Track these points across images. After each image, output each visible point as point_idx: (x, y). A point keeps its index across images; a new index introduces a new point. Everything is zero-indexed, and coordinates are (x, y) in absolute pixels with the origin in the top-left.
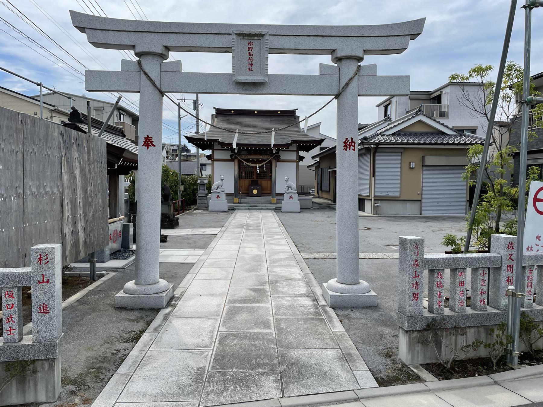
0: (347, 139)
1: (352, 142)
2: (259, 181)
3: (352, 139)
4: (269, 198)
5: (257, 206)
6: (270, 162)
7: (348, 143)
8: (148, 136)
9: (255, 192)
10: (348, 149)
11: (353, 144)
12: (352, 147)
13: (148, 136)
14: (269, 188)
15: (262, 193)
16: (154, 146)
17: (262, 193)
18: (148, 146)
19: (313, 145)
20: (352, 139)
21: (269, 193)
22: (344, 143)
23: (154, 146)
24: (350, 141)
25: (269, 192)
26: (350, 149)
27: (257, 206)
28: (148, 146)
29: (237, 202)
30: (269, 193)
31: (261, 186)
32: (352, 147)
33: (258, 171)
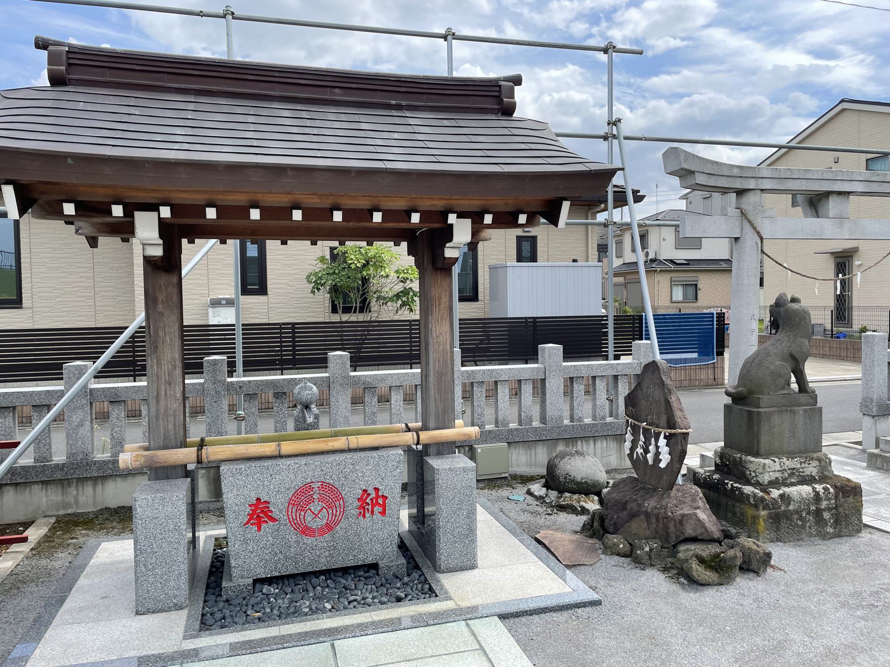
1: (377, 496)
7: (368, 501)
8: (258, 499)
11: (380, 501)
13: (258, 499)
16: (273, 519)
20: (377, 490)
26: (372, 513)
32: (377, 509)
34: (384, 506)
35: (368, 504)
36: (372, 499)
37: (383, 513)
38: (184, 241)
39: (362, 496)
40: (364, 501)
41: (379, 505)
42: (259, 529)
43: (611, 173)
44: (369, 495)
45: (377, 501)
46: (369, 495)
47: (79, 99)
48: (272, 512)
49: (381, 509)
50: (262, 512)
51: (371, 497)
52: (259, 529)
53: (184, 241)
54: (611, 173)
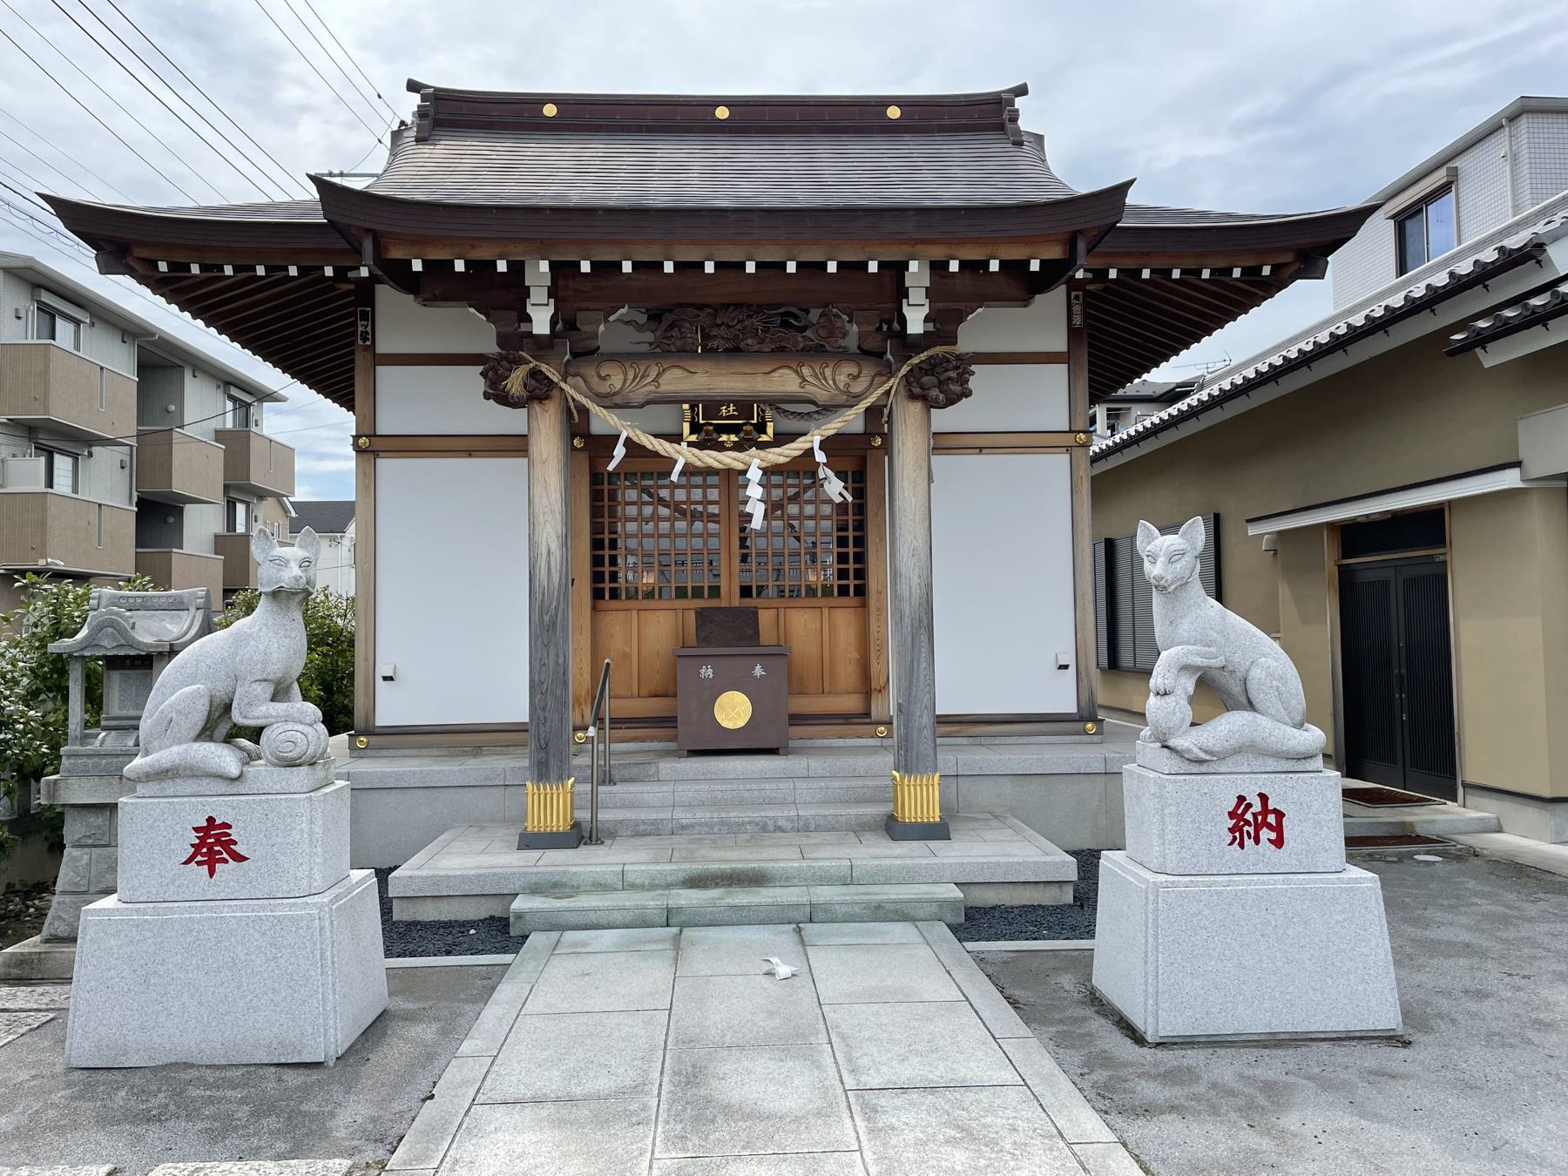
0: (1241, 799)
1: (1265, 811)
2: (765, 618)
3: (1264, 798)
4: (863, 763)
5: (756, 879)
6: (861, 457)
7: (1249, 816)
8: (211, 820)
9: (734, 710)
10: (1248, 842)
11: (1271, 819)
12: (1266, 834)
13: (211, 820)
14: (847, 673)
15: (797, 719)
16: (240, 858)
17: (797, 719)
18: (211, 864)
19: (1251, 272)
20: (1264, 798)
21: (846, 718)
22: (1232, 815)
23: (240, 858)
24: (1257, 807)
25: (851, 703)
26: (1257, 841)
27: (756, 879)
28: (211, 864)
29: (558, 822)
30: (846, 718)
31: (779, 653)
32: (1266, 834)
33: (757, 510)
34: (1279, 828)
35: (1247, 823)
36: (1255, 815)
37: (1279, 842)
38: (481, 368)
39: (1238, 806)
40: (1241, 817)
41: (1270, 827)
42: (212, 873)
43: (1124, 188)
44: (1249, 806)
45: (1265, 818)
46: (1249, 806)
47: (443, 151)
48: (235, 843)
49: (1273, 836)
50: (218, 842)
51: (1252, 810)
52: (212, 873)
53: (481, 368)
54: (1124, 188)
